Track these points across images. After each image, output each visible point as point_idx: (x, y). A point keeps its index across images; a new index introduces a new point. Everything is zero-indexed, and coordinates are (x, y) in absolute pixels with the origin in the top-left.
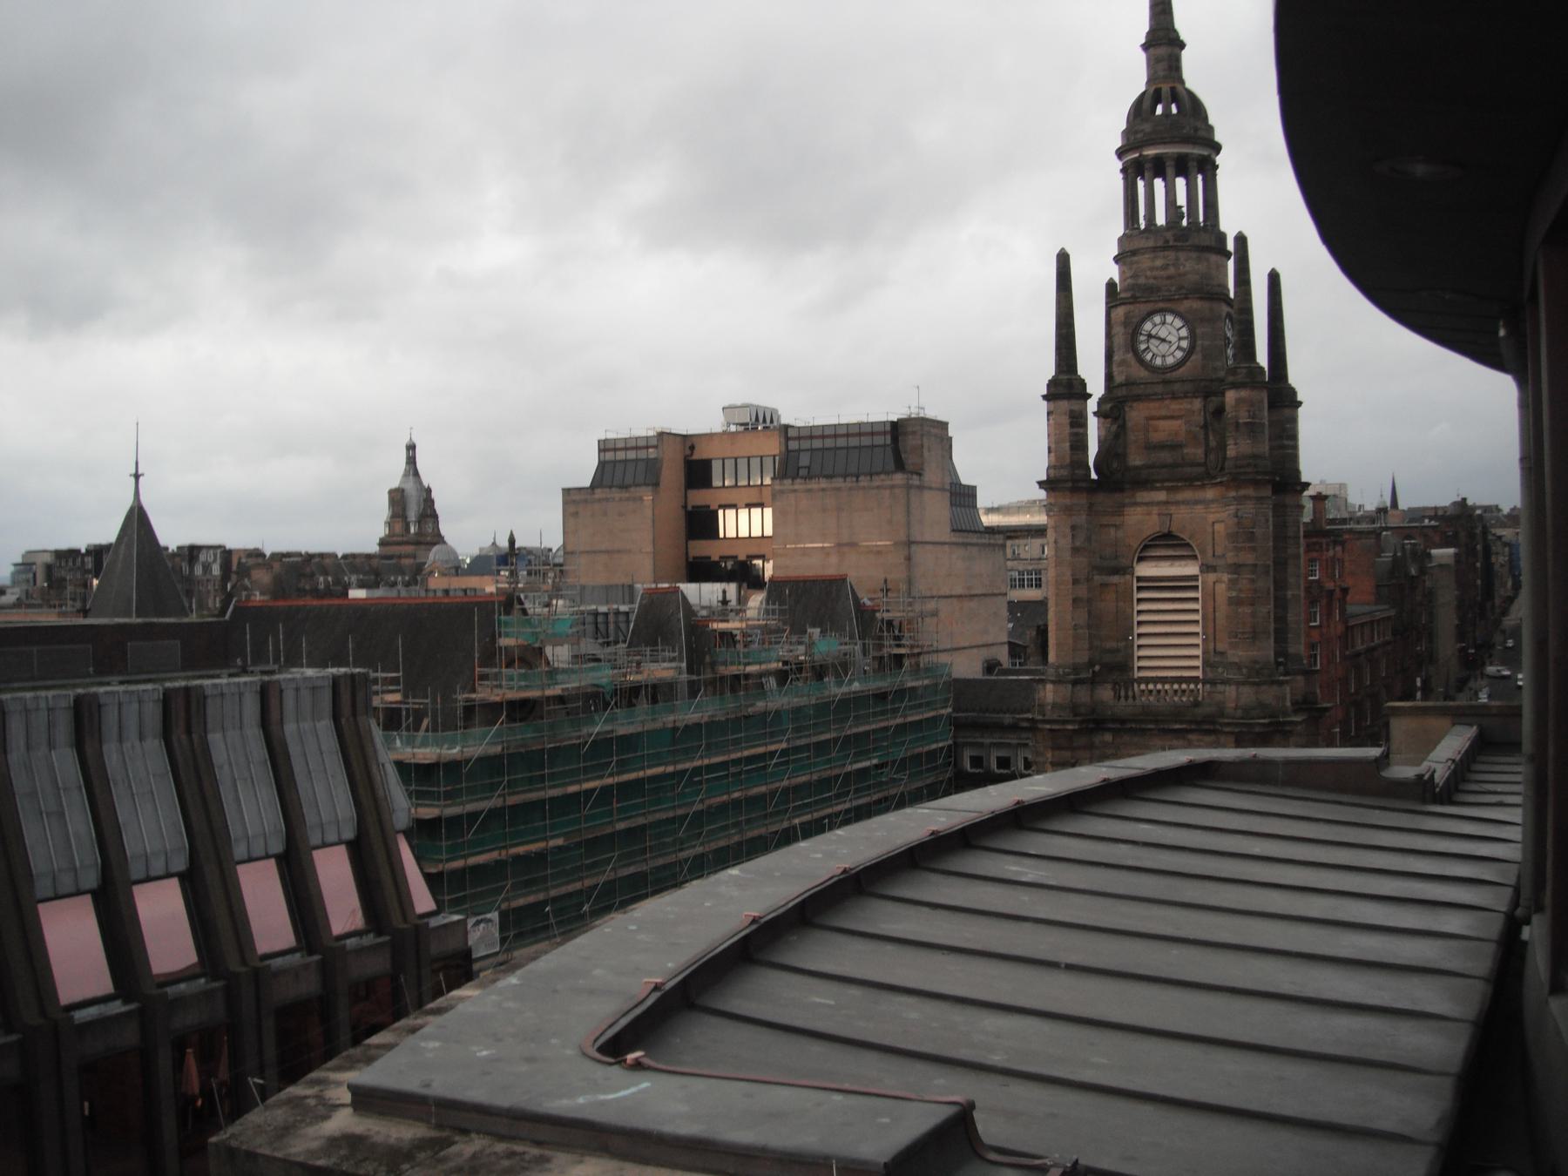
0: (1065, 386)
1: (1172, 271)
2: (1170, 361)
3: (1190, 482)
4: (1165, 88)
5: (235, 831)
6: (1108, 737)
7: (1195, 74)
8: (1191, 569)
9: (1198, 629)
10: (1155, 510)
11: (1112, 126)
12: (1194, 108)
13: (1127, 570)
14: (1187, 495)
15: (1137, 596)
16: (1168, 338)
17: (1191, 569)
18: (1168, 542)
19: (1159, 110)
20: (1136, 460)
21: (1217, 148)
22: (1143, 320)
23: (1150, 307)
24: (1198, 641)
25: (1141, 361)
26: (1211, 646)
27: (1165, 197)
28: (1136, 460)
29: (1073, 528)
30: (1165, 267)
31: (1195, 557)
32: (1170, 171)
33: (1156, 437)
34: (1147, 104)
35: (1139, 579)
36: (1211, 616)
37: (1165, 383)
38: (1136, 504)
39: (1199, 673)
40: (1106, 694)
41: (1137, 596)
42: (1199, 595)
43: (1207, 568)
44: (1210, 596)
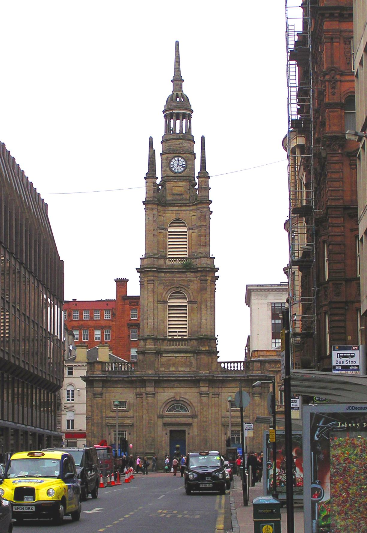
0: (151, 175)
1: (181, 145)
2: (180, 171)
3: (185, 205)
4: (179, 93)
5: (225, 390)
6: (163, 274)
7: (186, 89)
8: (185, 229)
9: (187, 250)
10: (174, 212)
11: (162, 104)
12: (187, 100)
13: (166, 229)
15: (168, 237)
16: (177, 164)
17: (185, 229)
18: (178, 221)
19: (178, 99)
20: (169, 198)
21: (192, 111)
22: (172, 159)
23: (175, 155)
24: (187, 250)
25: (171, 170)
26: (191, 251)
27: (178, 125)
28: (169, 198)
29: (154, 214)
30: (179, 144)
31: (186, 226)
32: (181, 118)
33: (174, 191)
34: (174, 97)
35: (169, 232)
36: (191, 242)
37: (178, 177)
38: (168, 211)
39: (187, 256)
40: (161, 262)
41: (168, 237)
42: (187, 237)
43: (189, 229)
44: (191, 236)
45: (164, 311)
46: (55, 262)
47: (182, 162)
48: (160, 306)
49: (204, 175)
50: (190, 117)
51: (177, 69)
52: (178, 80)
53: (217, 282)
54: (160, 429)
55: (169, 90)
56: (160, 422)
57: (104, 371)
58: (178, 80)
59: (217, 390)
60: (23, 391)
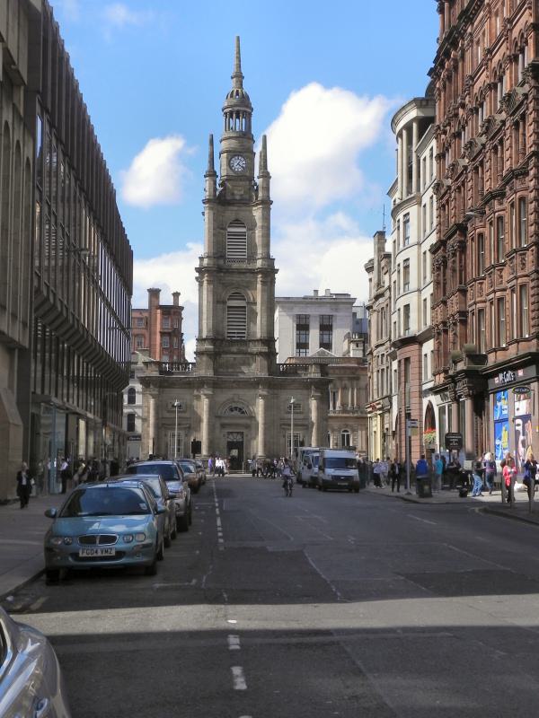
0: (212, 174)
8: (244, 230)
13: (225, 229)
14: (244, 208)
16: (239, 164)
17: (244, 230)
27: (239, 124)
40: (221, 262)
45: (224, 309)
46: (60, 77)
47: (243, 163)
48: (220, 306)
49: (266, 176)
50: (250, 114)
51: (239, 53)
52: (239, 77)
53: (276, 276)
54: (217, 431)
55: (231, 85)
56: (218, 425)
57: (161, 372)
58: (239, 77)
59: (276, 391)
60: (87, 374)
